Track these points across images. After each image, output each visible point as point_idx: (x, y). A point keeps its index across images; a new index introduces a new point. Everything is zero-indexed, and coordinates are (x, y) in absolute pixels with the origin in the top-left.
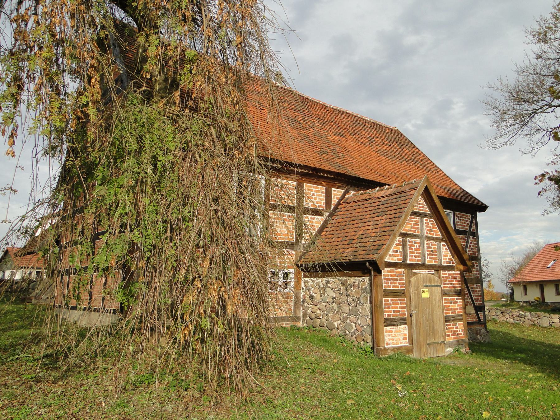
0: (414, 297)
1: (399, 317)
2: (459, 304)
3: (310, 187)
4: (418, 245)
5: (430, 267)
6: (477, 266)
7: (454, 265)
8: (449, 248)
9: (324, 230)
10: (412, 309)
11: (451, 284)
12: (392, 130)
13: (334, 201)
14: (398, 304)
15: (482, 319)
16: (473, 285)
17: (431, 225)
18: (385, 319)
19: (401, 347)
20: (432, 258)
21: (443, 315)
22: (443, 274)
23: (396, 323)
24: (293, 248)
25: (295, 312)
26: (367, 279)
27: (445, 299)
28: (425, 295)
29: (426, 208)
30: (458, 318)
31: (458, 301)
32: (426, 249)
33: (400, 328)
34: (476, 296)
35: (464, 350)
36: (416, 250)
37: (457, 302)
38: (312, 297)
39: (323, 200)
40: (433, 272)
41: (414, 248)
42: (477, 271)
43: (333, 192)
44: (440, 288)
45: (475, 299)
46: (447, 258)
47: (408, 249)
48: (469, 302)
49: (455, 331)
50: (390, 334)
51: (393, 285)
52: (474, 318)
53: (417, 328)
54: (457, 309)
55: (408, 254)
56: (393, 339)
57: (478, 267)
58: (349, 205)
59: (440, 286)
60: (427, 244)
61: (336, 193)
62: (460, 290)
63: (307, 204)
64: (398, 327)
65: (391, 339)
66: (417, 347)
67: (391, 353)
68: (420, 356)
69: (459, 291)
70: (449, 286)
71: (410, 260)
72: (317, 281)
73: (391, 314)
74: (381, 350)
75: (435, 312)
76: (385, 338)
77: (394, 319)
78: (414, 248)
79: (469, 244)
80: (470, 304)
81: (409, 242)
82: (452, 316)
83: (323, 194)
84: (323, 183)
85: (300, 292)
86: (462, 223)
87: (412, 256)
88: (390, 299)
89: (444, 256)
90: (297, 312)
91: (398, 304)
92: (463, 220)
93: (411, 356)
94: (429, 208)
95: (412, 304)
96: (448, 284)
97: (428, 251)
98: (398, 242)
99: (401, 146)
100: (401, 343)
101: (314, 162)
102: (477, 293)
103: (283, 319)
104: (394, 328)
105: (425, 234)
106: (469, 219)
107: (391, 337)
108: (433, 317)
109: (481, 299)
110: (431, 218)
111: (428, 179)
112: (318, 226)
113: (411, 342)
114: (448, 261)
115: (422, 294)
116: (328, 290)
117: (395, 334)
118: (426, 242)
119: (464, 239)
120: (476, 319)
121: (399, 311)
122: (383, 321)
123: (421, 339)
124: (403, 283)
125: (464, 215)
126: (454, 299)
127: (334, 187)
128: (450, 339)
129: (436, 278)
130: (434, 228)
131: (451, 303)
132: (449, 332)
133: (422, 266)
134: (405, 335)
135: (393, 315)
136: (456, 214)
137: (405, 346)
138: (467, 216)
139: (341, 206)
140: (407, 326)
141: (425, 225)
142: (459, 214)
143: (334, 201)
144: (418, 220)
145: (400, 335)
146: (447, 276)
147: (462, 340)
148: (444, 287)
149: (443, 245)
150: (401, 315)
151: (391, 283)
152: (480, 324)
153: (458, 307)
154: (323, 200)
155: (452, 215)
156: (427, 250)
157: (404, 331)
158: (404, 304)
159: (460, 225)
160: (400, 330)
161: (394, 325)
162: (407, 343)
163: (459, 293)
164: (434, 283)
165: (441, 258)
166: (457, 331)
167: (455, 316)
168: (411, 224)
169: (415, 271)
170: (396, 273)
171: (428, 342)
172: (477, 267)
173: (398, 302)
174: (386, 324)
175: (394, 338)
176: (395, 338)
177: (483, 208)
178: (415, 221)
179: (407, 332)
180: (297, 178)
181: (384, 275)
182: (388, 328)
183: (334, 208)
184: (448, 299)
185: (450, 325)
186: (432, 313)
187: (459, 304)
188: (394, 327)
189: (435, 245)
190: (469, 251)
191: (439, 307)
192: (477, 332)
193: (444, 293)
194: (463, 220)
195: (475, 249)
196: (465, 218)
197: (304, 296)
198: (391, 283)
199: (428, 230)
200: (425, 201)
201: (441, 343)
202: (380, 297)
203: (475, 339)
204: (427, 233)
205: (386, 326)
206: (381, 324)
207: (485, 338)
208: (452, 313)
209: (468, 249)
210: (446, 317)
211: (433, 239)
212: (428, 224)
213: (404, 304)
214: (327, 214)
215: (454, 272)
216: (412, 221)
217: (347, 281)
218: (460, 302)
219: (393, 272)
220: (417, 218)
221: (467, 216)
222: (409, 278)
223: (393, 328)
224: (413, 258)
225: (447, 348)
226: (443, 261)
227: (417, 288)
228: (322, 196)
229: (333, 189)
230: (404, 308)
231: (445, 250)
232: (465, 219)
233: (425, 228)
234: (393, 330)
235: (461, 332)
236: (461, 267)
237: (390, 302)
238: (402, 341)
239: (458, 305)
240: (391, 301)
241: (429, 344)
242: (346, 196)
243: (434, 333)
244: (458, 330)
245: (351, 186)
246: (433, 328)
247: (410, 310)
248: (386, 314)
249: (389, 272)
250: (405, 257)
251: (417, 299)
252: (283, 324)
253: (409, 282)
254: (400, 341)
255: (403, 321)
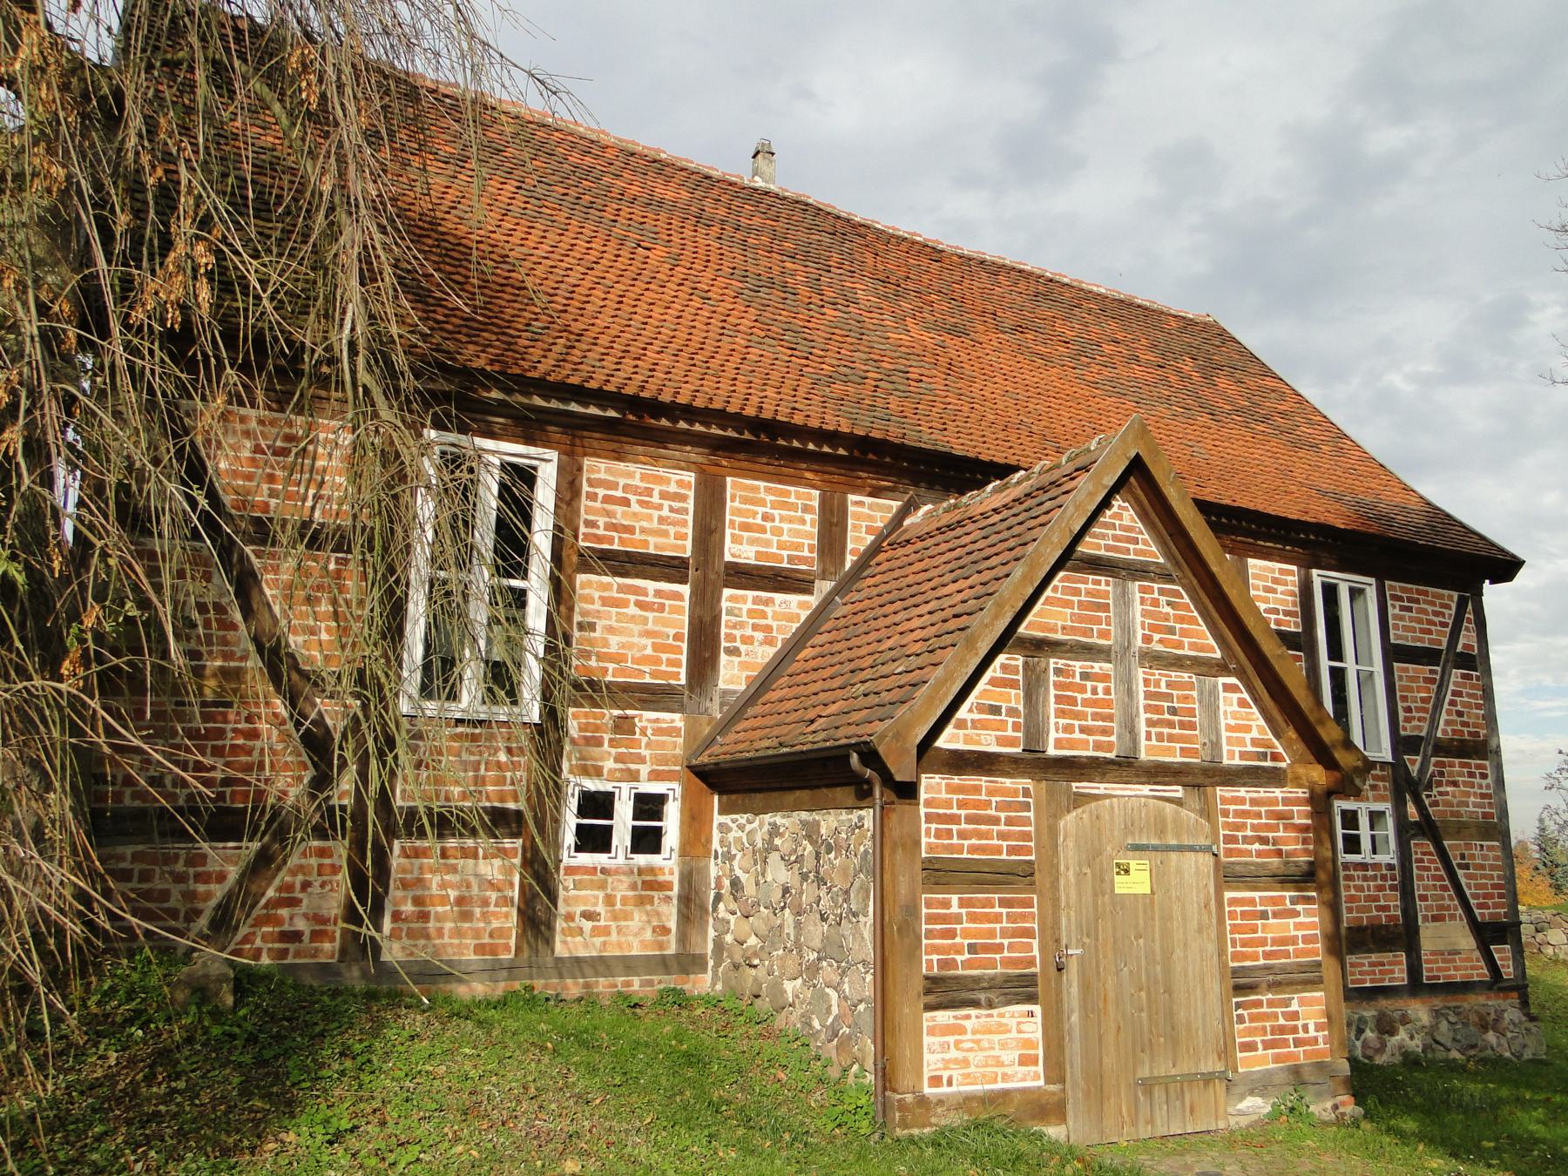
0: (1073, 892)
1: (999, 970)
2: (1301, 919)
3: (757, 489)
4: (1100, 686)
5: (1158, 773)
6: (1484, 776)
7: (1283, 765)
8: (1255, 701)
9: (809, 644)
10: (1064, 941)
11: (1264, 841)
12: (1187, 324)
13: (858, 540)
14: (997, 918)
15: (1508, 971)
16: (1469, 847)
17: (1168, 609)
18: (927, 978)
19: (1006, 1093)
20: (1171, 738)
21: (1223, 965)
22: (1224, 801)
23: (982, 996)
24: (676, 706)
25: (683, 938)
26: (868, 816)
27: (1233, 902)
28: (1136, 881)
29: (1145, 542)
30: (1306, 978)
31: (1299, 907)
32: (1142, 702)
33: (1002, 1015)
34: (1477, 886)
35: (1329, 1105)
36: (1086, 703)
37: (1297, 914)
38: (736, 884)
39: (809, 535)
40: (1178, 791)
41: (1079, 696)
42: (1483, 796)
43: (851, 508)
44: (1209, 859)
45: (1476, 896)
46: (1248, 737)
47: (1052, 699)
48: (1448, 908)
49: (1282, 1030)
50: (951, 1039)
51: (974, 841)
52: (1473, 968)
53: (1085, 1017)
54: (1294, 940)
55: (1052, 720)
56: (965, 1063)
57: (1489, 780)
58: (900, 552)
59: (1207, 849)
60: (1147, 682)
61: (865, 510)
62: (1311, 863)
63: (739, 550)
64: (995, 1012)
65: (956, 1061)
66: (1087, 1094)
67: (955, 1119)
68: (1102, 1133)
69: (1305, 867)
70: (1257, 846)
71: (1059, 744)
72: (749, 827)
73: (959, 958)
74: (902, 1106)
75: (1178, 953)
76: (927, 1057)
77: (976, 980)
78: (1079, 696)
79: (1449, 697)
80: (1452, 917)
81: (1058, 672)
82: (1266, 967)
83: (808, 517)
84: (808, 475)
85: (707, 867)
86: (1420, 621)
87: (1068, 729)
88: (955, 898)
89: (1229, 728)
90: (694, 938)
91: (997, 918)
92: (1424, 611)
93: (1054, 1132)
94: (1162, 543)
95: (1064, 921)
96: (1246, 840)
97: (1148, 708)
98: (999, 674)
99: (1210, 370)
100: (1005, 1077)
101: (771, 404)
102: (1483, 877)
103: (629, 965)
104: (973, 1018)
105: (1139, 642)
106: (1448, 607)
107: (954, 1054)
108: (1167, 971)
109: (1501, 896)
110: (1172, 581)
111: (1143, 431)
112: (785, 631)
113: (1055, 1069)
114: (1250, 748)
115: (1117, 879)
116: (774, 857)
117: (978, 1042)
118: (1140, 674)
119: (1426, 680)
120: (1481, 972)
121: (999, 948)
122: (918, 985)
123: (1109, 1061)
124: (1026, 836)
125: (1426, 593)
126: (1274, 901)
127: (857, 489)
128: (1258, 1061)
129: (1189, 815)
130: (1181, 619)
131: (1264, 915)
132: (1250, 1032)
133: (1125, 767)
134: (1028, 1044)
135: (967, 964)
136: (1392, 588)
137: (1024, 1091)
138: (1441, 597)
139: (881, 557)
140: (1037, 1009)
141: (1138, 608)
142: (1404, 590)
143: (858, 540)
144: (1103, 587)
145: (1004, 1046)
146: (1247, 807)
147: (1320, 1066)
148: (1229, 853)
149: (1228, 688)
150: (1007, 962)
151: (963, 835)
152: (1501, 989)
153: (1300, 933)
154: (809, 535)
155: (1371, 594)
156: (680, 666)
157: (1023, 1027)
158: (1023, 917)
159: (1406, 628)
160: (1000, 1025)
161: (975, 1004)
162: (1037, 1077)
163: (1303, 878)
164: (1178, 836)
165: (1218, 736)
166: (1294, 1030)
167: (1284, 970)
168: (1069, 604)
169: (1077, 786)
170: (990, 793)
171: (1144, 1072)
172: (1484, 782)
173: (997, 909)
174: (931, 999)
175: (971, 1056)
176: (976, 1058)
177: (1505, 567)
178: (1088, 593)
179: (1039, 1035)
180: (700, 459)
181: (928, 803)
182: (944, 1017)
183: (854, 564)
184: (1252, 902)
185: (1259, 1004)
186: (1168, 955)
187: (1301, 919)
188: (973, 1012)
189: (1190, 686)
190: (1448, 723)
191: (1200, 930)
192: (1482, 1018)
193: (1229, 876)
194: (1424, 611)
195: (1477, 716)
196: (1432, 604)
197: (718, 879)
198: (963, 835)
199: (1154, 628)
200: (1143, 516)
201: (1208, 1079)
202: (903, 890)
203: (1474, 1046)
204: (1147, 639)
205: (929, 1008)
206: (907, 1003)
207: (1520, 1040)
208: (1267, 955)
209: (1444, 716)
210: (1236, 972)
211: (1178, 663)
212: (1155, 603)
213: (1023, 917)
214: (824, 587)
215: (1278, 793)
216: (1077, 592)
217: (817, 824)
218: (1308, 913)
219: (977, 789)
220: (1098, 583)
221: (1441, 597)
222: (1056, 816)
223: (968, 1017)
224: (1077, 735)
225: (1242, 1097)
226: (1225, 748)
227: (1093, 855)
228: (803, 522)
229: (852, 497)
230: (1028, 933)
231: (1236, 708)
232: (1430, 608)
233: (1139, 619)
234: (968, 1024)
235: (1312, 1033)
236: (1318, 774)
237: (955, 909)
238: (1009, 1071)
239: (1298, 926)
240: (961, 906)
241: (1148, 1085)
242: (907, 522)
243: (1174, 1042)
244: (1300, 1023)
245: (930, 487)
246: (1170, 1014)
247: (1052, 940)
248: (935, 957)
249: (951, 789)
250: (1034, 730)
251: (1088, 898)
252: (628, 984)
253: (1053, 832)
254: (1000, 1070)
255: (1020, 988)
